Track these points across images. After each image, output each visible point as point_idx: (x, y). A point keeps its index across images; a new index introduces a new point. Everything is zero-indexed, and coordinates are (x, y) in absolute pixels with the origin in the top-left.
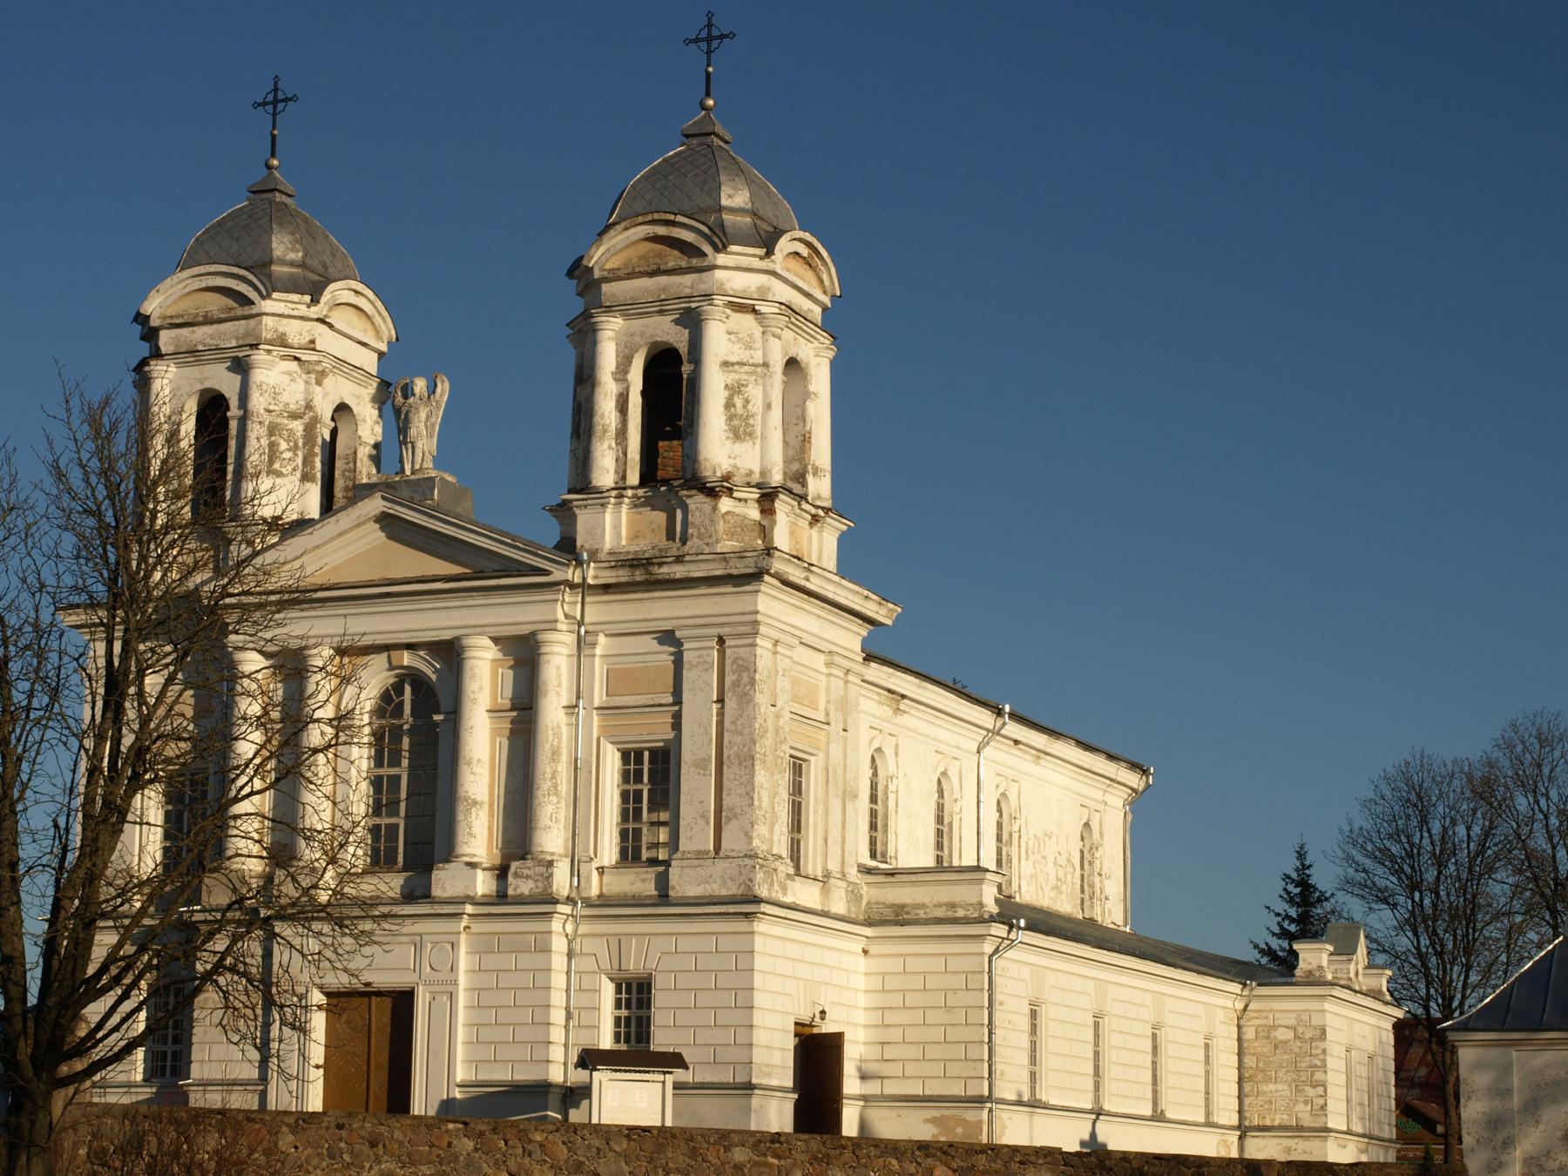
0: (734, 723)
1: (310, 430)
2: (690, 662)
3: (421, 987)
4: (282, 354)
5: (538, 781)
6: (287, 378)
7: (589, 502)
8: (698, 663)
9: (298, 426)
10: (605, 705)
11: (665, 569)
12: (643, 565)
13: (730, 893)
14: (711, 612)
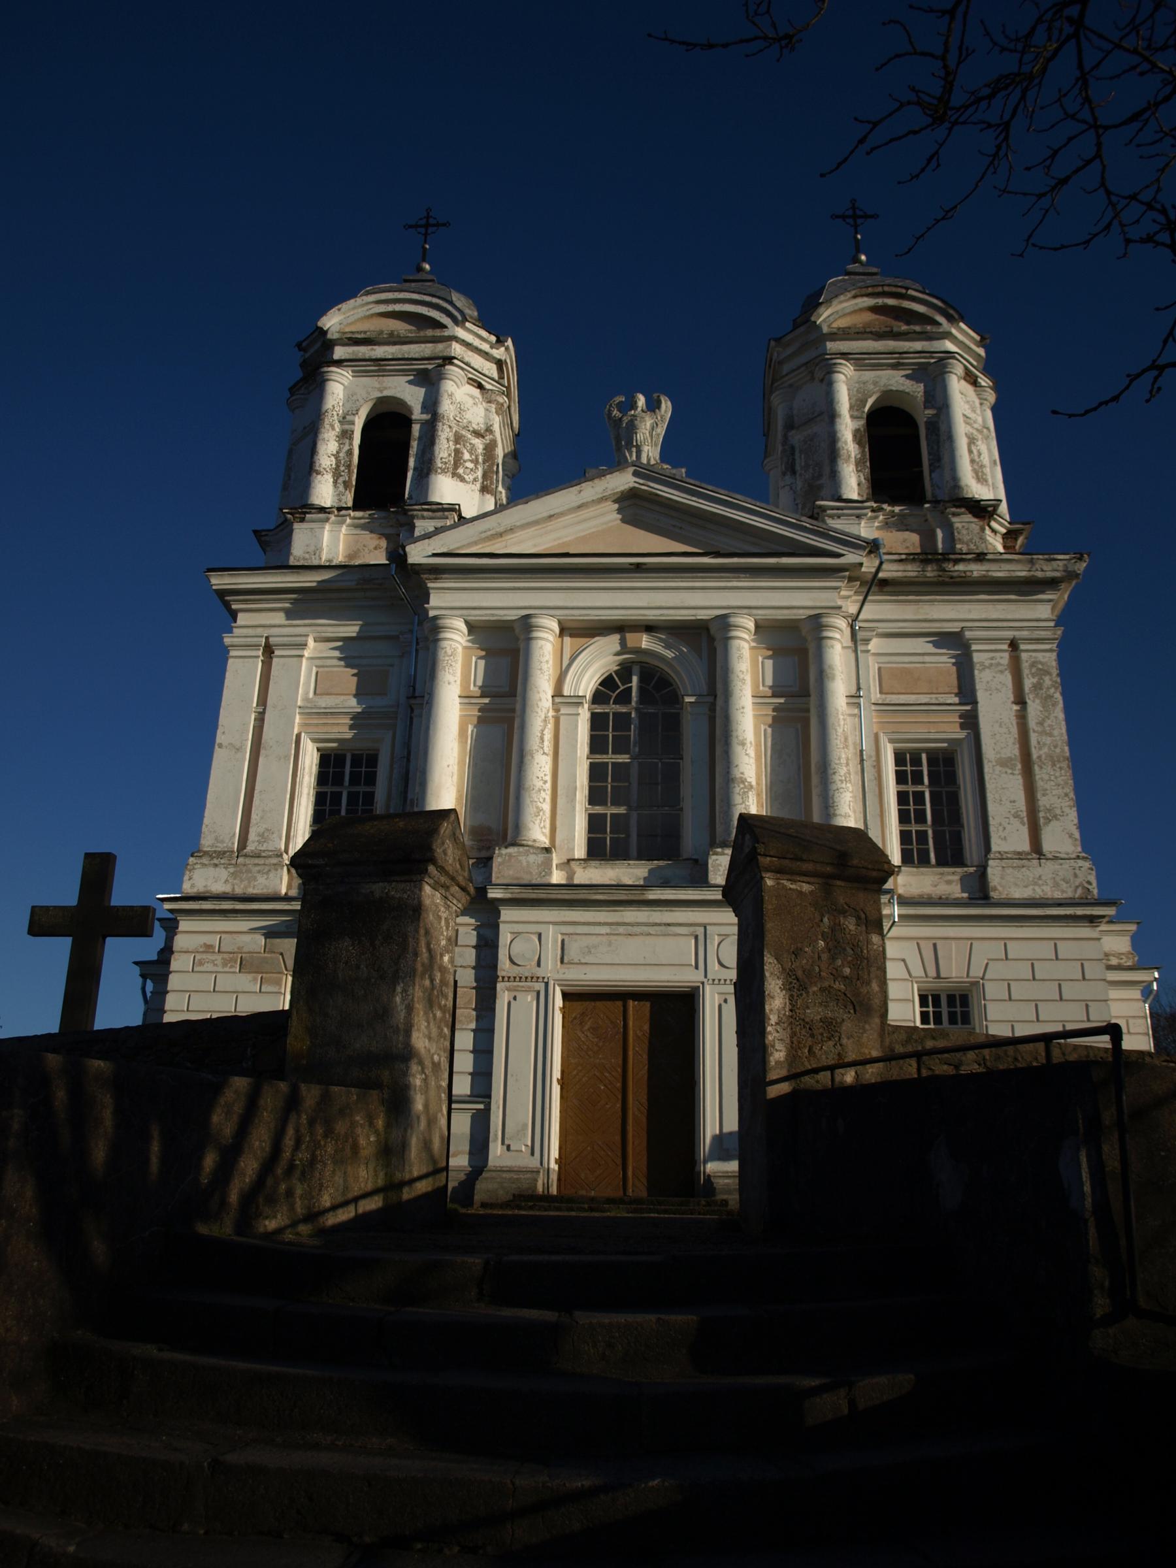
0: (1041, 723)
1: (490, 448)
2: (982, 664)
3: (708, 988)
4: (470, 376)
5: (833, 765)
6: (471, 401)
7: (845, 511)
8: (991, 665)
9: (479, 444)
10: (880, 702)
11: (961, 567)
12: (938, 560)
13: (1065, 896)
14: (1002, 617)
